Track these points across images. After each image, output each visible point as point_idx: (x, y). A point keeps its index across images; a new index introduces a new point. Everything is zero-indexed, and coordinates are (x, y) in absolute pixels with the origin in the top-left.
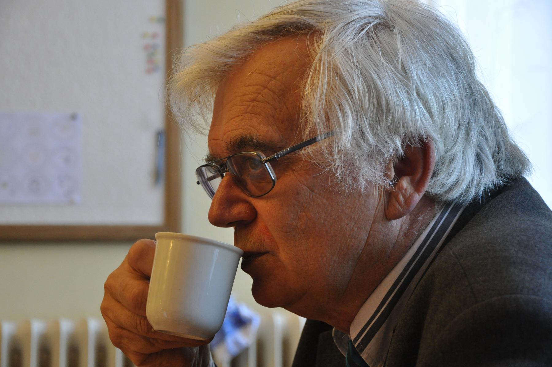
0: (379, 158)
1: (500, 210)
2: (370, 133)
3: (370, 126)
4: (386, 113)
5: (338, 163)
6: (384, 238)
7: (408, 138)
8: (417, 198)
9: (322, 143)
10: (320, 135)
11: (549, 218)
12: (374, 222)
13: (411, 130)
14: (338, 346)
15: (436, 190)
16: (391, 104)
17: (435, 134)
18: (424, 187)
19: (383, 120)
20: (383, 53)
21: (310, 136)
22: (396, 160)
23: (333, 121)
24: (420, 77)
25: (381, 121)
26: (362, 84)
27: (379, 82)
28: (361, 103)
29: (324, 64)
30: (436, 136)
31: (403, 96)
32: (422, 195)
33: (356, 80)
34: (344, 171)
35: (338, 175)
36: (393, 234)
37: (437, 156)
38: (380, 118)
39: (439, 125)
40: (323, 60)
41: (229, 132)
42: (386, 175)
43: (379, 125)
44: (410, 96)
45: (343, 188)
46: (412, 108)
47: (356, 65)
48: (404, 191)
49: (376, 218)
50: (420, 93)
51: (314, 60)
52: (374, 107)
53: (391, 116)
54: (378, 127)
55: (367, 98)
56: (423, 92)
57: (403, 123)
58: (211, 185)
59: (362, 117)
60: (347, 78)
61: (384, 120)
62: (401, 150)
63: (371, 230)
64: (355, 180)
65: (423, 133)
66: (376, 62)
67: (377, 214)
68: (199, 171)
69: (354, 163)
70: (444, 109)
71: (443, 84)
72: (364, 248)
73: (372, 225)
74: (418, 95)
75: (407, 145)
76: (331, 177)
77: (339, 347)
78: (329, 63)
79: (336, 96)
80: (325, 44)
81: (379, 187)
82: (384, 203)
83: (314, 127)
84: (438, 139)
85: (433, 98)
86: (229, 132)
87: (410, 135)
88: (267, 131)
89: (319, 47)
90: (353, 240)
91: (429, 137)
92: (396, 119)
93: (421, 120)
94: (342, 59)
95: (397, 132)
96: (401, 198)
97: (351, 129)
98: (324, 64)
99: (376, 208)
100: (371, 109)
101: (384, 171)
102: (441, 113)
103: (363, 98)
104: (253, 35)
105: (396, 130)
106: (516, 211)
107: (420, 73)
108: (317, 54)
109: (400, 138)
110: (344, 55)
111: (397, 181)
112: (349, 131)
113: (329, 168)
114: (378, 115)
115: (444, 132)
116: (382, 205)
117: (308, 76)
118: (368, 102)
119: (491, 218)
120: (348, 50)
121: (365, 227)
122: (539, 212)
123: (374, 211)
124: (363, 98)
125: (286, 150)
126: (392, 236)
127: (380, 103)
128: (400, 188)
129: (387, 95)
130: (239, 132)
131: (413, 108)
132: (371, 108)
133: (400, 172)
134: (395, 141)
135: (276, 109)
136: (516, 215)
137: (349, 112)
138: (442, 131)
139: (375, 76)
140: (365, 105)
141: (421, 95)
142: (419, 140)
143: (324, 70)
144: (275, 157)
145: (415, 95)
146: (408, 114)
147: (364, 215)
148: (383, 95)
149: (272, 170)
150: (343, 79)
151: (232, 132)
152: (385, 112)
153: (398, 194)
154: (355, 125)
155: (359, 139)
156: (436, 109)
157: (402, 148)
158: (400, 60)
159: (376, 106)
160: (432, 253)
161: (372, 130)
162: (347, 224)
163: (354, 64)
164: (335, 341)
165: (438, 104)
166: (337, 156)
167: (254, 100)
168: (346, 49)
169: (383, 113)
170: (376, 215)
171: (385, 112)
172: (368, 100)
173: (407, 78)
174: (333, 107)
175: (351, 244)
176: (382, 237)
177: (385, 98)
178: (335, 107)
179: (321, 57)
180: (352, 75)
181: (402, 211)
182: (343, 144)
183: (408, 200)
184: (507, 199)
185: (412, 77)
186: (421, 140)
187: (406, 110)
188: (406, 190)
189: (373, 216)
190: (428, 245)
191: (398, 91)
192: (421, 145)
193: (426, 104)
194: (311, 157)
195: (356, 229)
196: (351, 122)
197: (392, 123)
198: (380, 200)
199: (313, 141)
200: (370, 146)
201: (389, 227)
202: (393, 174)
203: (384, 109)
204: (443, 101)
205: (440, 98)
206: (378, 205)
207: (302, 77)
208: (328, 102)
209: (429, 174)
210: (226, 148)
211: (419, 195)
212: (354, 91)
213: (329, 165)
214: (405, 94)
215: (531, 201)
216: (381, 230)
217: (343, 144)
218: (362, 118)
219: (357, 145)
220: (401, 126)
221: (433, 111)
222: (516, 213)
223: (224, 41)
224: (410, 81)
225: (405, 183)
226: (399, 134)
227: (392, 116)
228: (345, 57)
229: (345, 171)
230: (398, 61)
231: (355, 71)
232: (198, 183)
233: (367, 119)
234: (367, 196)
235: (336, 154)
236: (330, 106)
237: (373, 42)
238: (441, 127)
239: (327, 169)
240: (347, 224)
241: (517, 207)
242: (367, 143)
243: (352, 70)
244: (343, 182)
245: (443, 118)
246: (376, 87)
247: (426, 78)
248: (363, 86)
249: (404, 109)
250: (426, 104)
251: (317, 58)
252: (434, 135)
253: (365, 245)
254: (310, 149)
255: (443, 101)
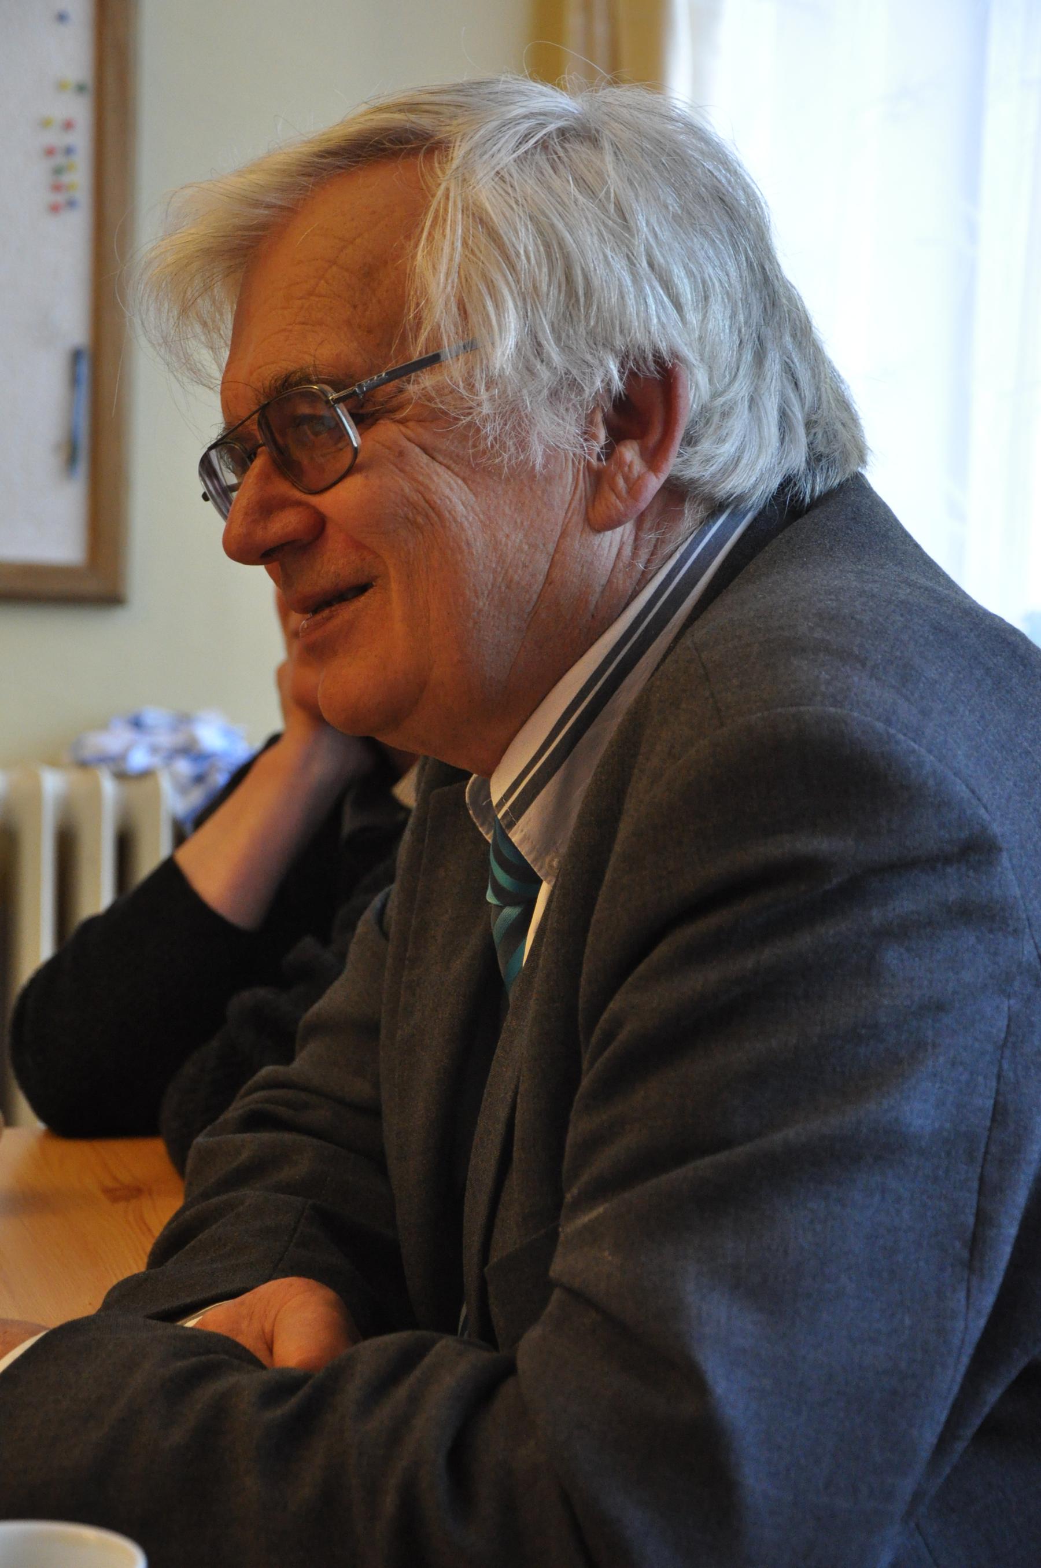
0: (573, 397)
1: (798, 548)
2: (552, 343)
3: (553, 330)
4: (586, 301)
5: (486, 409)
6: (585, 571)
7: (632, 357)
8: (654, 484)
9: (454, 370)
10: (449, 345)
11: (901, 560)
12: (563, 534)
13: (636, 338)
14: (478, 824)
15: (692, 472)
16: (596, 282)
17: (688, 350)
18: (667, 460)
19: (579, 317)
20: (575, 179)
21: (427, 353)
22: (608, 407)
23: (475, 318)
24: (654, 229)
25: (575, 318)
26: (534, 240)
27: (567, 235)
28: (533, 281)
29: (455, 202)
30: (690, 354)
31: (619, 265)
32: (663, 478)
33: (522, 233)
34: (499, 424)
35: (486, 433)
36: (602, 563)
37: (694, 401)
38: (572, 312)
39: (697, 333)
40: (452, 195)
41: (260, 367)
42: (588, 435)
43: (572, 327)
44: (635, 265)
45: (497, 461)
46: (639, 293)
47: (520, 203)
48: (626, 469)
49: (567, 526)
50: (655, 263)
51: (433, 196)
52: (560, 291)
53: (595, 308)
54: (568, 330)
55: (545, 270)
56: (662, 261)
57: (621, 324)
58: (225, 479)
59: (534, 309)
60: (502, 227)
61: (582, 317)
62: (618, 384)
63: (556, 551)
64: (522, 445)
65: (663, 347)
66: (560, 197)
67: (570, 518)
68: (207, 468)
69: (521, 409)
70: (706, 298)
71: (703, 249)
72: (542, 590)
73: (558, 541)
74: (651, 265)
75: (632, 374)
76: (473, 436)
77: (482, 825)
78: (465, 200)
79: (481, 264)
80: (456, 163)
81: (573, 460)
82: (586, 496)
83: (436, 329)
84: (694, 362)
85: (683, 274)
86: (260, 367)
87: (636, 349)
88: (337, 355)
89: (444, 173)
90: (520, 571)
91: (675, 355)
92: (607, 315)
93: (659, 318)
94: (492, 192)
95: (608, 344)
96: (621, 483)
97: (513, 333)
98: (455, 202)
99: (566, 506)
100: (552, 296)
101: (584, 425)
102: (700, 305)
103: (536, 270)
104: (311, 159)
105: (606, 339)
106: (832, 550)
107: (653, 220)
108: (440, 185)
109: (617, 356)
110: (496, 183)
111: (610, 451)
112: (509, 338)
113: (470, 417)
114: (568, 307)
115: (707, 349)
116: (581, 500)
117: (423, 229)
118: (547, 278)
119: (778, 567)
120: (502, 173)
121: (544, 545)
122: (882, 547)
123: (564, 512)
124: (536, 270)
125: (378, 377)
126: (600, 567)
127: (573, 281)
128: (621, 464)
129: (587, 264)
130: (280, 367)
131: (641, 292)
132: (553, 292)
133: (617, 435)
134: (605, 363)
135: (355, 307)
136: (830, 559)
137: (510, 304)
138: (703, 345)
139: (560, 225)
140: (541, 285)
141: (656, 266)
142: (655, 362)
143: (455, 215)
144: (355, 391)
145: (645, 264)
146: (631, 301)
147: (543, 518)
148: (578, 263)
149: (352, 423)
150: (497, 233)
151: (267, 367)
152: (582, 300)
153: (615, 475)
154: (522, 326)
155: (532, 358)
156: (689, 296)
157: (621, 379)
158: (612, 195)
159: (563, 288)
160: (670, 626)
161: (558, 339)
162: (507, 536)
163: (517, 202)
164: (471, 812)
165: (695, 289)
166: (484, 395)
167: (311, 293)
168: (498, 173)
169: (577, 300)
170: (567, 520)
171: (582, 300)
172: (547, 274)
173: (627, 228)
174: (474, 288)
175: (516, 578)
176: (580, 569)
177: (583, 269)
178: (479, 291)
179: (448, 189)
180: (513, 223)
181: (622, 508)
182: (498, 366)
183: (634, 488)
184: (816, 524)
185: (637, 225)
186: (659, 360)
187: (626, 296)
188: (630, 466)
189: (560, 523)
190: (657, 613)
191: (610, 257)
192: (659, 373)
193: (667, 285)
194: (431, 396)
195: (526, 547)
196: (512, 320)
197: (597, 322)
198: (576, 488)
199: (433, 360)
200: (553, 370)
201: (596, 547)
202: (602, 434)
203: (581, 292)
204: (704, 282)
205: (698, 276)
206: (572, 499)
207: (408, 237)
208: (463, 280)
209: (676, 434)
210: (256, 401)
211: (657, 477)
212: (518, 255)
213: (470, 414)
214: (624, 262)
215: (867, 524)
216: (578, 552)
217: (498, 366)
218: (535, 311)
219: (528, 369)
220: (618, 329)
221: (683, 300)
222: (831, 553)
223: (253, 177)
224: (633, 236)
225: (630, 453)
226: (613, 349)
227: (598, 308)
228: (497, 187)
229: (502, 424)
230: (608, 198)
231: (518, 214)
232: (205, 497)
233: (545, 315)
234: (549, 479)
235: (482, 390)
236: (470, 288)
237: (557, 160)
238: (700, 338)
239: (464, 421)
240: (507, 536)
241: (835, 540)
242: (547, 364)
243: (512, 212)
244: (497, 446)
245: (705, 316)
246: (561, 245)
247: (667, 233)
248: (536, 244)
249: (622, 296)
250: (667, 285)
251: (440, 192)
252: (687, 351)
253: (545, 583)
254: (427, 380)
255: (704, 282)
